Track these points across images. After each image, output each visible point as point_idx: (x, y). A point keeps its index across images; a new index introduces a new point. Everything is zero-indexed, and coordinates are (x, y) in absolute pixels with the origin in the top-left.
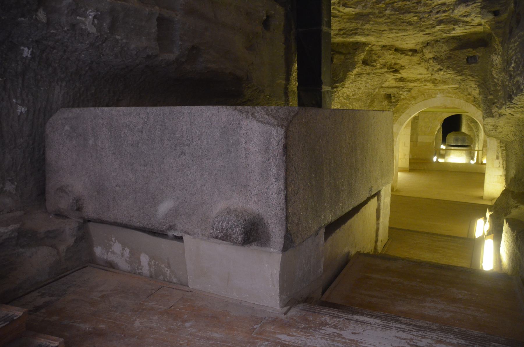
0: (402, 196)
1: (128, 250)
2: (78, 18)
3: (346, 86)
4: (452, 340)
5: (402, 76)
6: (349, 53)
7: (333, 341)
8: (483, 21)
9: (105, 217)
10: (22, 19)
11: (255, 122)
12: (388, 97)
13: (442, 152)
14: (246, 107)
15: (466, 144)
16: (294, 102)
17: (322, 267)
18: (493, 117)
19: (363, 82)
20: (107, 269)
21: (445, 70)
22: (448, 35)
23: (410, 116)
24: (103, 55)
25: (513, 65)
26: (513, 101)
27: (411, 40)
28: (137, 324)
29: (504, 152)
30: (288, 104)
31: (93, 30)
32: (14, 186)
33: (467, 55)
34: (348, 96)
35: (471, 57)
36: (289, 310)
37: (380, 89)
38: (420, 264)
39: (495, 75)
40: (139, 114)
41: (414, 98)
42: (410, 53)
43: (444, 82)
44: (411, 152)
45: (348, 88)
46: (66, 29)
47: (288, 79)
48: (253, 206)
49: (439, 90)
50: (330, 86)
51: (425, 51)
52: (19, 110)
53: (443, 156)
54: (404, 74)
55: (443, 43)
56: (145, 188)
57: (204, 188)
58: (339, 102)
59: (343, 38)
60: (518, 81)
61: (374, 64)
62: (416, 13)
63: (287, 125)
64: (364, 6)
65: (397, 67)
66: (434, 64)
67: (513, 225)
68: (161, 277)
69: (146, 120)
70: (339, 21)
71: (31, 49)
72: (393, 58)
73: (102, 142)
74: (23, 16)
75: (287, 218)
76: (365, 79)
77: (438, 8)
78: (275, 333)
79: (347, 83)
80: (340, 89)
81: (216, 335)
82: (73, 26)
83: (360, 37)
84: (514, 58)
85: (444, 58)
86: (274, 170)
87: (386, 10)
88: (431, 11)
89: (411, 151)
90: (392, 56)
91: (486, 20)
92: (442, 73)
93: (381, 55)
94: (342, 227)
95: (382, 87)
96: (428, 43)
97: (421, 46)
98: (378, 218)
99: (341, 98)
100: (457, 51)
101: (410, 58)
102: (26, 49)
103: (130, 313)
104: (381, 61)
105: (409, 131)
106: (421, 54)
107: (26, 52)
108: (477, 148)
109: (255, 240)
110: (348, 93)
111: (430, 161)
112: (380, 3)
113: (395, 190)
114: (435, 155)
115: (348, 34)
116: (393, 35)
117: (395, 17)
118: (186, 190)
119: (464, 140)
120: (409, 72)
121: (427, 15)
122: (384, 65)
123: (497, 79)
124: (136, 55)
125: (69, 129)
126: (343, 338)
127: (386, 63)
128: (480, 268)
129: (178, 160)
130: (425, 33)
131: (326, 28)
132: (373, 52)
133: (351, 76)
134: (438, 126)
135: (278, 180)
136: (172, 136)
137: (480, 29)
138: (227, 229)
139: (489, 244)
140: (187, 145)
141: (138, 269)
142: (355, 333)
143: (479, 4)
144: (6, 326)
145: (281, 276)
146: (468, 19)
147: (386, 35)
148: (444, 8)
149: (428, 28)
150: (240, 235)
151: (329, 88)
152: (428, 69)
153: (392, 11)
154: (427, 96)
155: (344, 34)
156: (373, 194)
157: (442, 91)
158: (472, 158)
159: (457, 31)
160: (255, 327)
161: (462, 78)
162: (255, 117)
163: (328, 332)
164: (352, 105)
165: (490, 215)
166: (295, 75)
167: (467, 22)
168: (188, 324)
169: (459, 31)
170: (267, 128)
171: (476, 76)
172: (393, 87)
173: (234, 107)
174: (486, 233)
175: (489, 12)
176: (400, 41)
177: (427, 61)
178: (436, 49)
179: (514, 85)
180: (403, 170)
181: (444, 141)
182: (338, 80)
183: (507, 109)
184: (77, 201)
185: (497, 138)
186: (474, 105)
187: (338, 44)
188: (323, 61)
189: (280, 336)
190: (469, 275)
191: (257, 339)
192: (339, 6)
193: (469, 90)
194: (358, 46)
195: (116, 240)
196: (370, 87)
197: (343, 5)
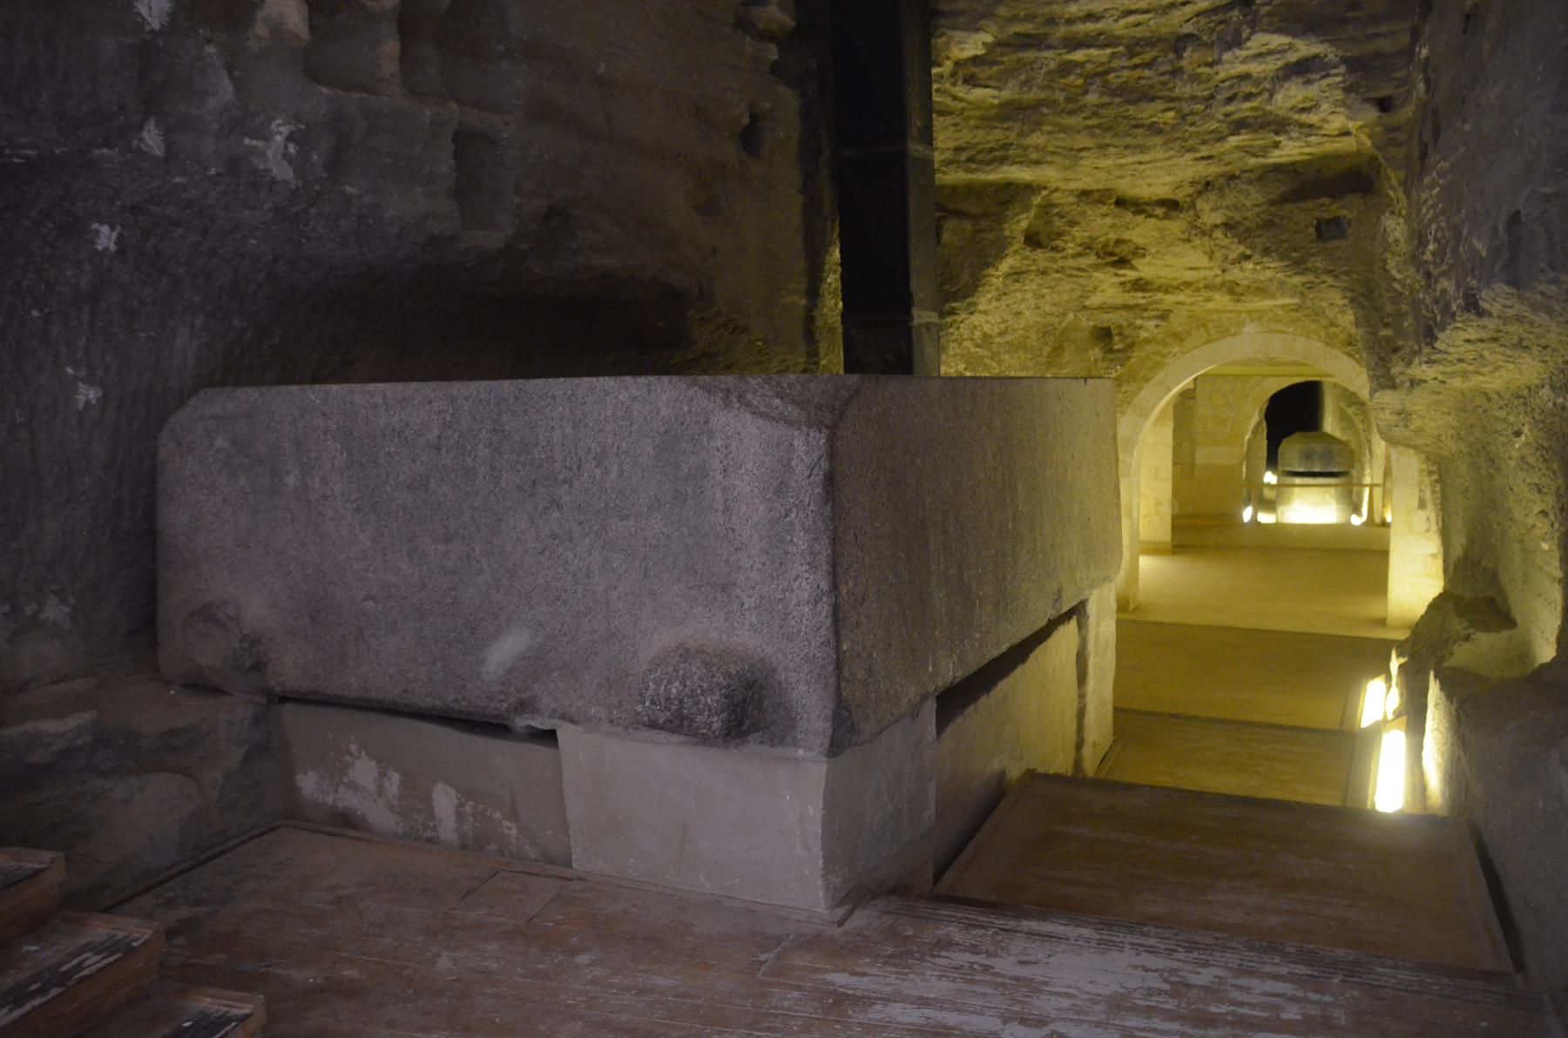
0: (1154, 623)
1: (396, 778)
2: (247, 141)
3: (981, 307)
4: (1276, 969)
5: (1142, 275)
6: (986, 215)
7: (972, 982)
8: (1352, 126)
9: (351, 682)
10: (105, 151)
11: (748, 416)
12: (1104, 335)
13: (1268, 494)
14: (722, 378)
15: (1336, 469)
16: (833, 357)
17: (933, 805)
18: (1394, 387)
19: (1029, 295)
20: (336, 830)
21: (1257, 257)
22: (1261, 160)
23: (1169, 390)
24: (309, 239)
25: (1431, 247)
26: (1437, 345)
27: (1160, 174)
28: (444, 963)
29: (1438, 488)
30: (816, 363)
31: (283, 172)
32: (66, 609)
33: (1317, 214)
34: (986, 336)
35: (1329, 222)
36: (852, 911)
37: (1080, 315)
38: (1200, 797)
39: (1394, 272)
40: (430, 402)
41: (1178, 337)
42: (1160, 211)
43: (1261, 291)
44: (1175, 495)
45: (985, 312)
46: (213, 171)
47: (813, 293)
48: (746, 637)
49: (1249, 312)
50: (935, 310)
51: (1200, 204)
52: (82, 398)
53: (1270, 506)
54: (1145, 269)
55: (1250, 182)
56: (449, 600)
57: (614, 595)
58: (962, 356)
59: (967, 171)
60: (1444, 292)
61: (1058, 242)
62: (1172, 100)
63: (831, 420)
64: (1025, 83)
65: (1124, 250)
66: (1226, 242)
67: (1448, 687)
68: (493, 847)
69: (448, 418)
70: (956, 125)
71: (118, 229)
72: (1113, 226)
73: (324, 480)
74: (107, 143)
75: (839, 666)
76: (1034, 286)
77: (1232, 86)
78: (816, 970)
79: (982, 300)
80: (963, 316)
81: (660, 981)
82: (234, 165)
83: (1015, 168)
84: (1433, 227)
85: (1253, 225)
86: (801, 541)
87: (1086, 92)
88: (1212, 97)
89: (1176, 494)
90: (1108, 221)
91: (1359, 123)
92: (1249, 265)
93: (1077, 219)
94: (983, 700)
95: (1085, 308)
96: (1208, 184)
97: (1190, 190)
98: (1082, 678)
99: (966, 343)
100: (1287, 207)
101: (1161, 224)
102: (105, 229)
103: (420, 938)
104: (1078, 233)
105: (1167, 432)
106: (1191, 212)
107: (106, 238)
108: (1367, 480)
109: (755, 728)
110: (986, 328)
111: (1233, 520)
112: (1069, 73)
113: (1132, 606)
114: (1247, 502)
115: (981, 162)
116: (1109, 162)
117: (1112, 111)
118: (565, 602)
119: (1328, 456)
120: (1159, 262)
121: (1200, 107)
122: (1087, 247)
123: (1399, 281)
124: (398, 236)
125: (227, 445)
126: (997, 975)
127: (1091, 238)
128: (1369, 806)
129: (540, 522)
130: (1198, 155)
131: (920, 148)
132: (1056, 210)
133: (994, 281)
134: (1254, 417)
135: (813, 566)
136: (522, 458)
137: (1348, 145)
138: (681, 702)
139: (1393, 745)
140: (564, 482)
141: (425, 827)
142: (1027, 963)
143: (1339, 79)
144: (43, 1004)
145: (828, 823)
146: (1312, 118)
147: (1088, 161)
148: (1248, 88)
149: (1204, 142)
150: (717, 714)
151: (933, 317)
152: (1211, 255)
153: (1102, 94)
154: (1213, 329)
155: (970, 160)
156: (1065, 609)
157: (1259, 316)
158: (1356, 509)
159: (1286, 151)
160: (763, 957)
161: (1305, 279)
162: (749, 405)
163: (954, 963)
164: (1000, 362)
165: (1401, 667)
166: (833, 279)
167: (1311, 126)
168: (582, 959)
169: (1290, 150)
170: (779, 431)
171: (1345, 273)
172: (1116, 308)
173: (689, 379)
174: (1390, 717)
175: (1366, 100)
176: (1128, 179)
177: (1205, 233)
178: (1230, 199)
179: (1436, 302)
180: (1154, 549)
181: (1272, 461)
182: (956, 290)
183: (1424, 367)
184: (253, 643)
185: (1416, 448)
186: (1349, 354)
187: (954, 189)
188: (913, 240)
189: (830, 977)
190: (1337, 828)
191: (771, 985)
192: (954, 84)
193: (1330, 313)
194: (1012, 194)
195: (360, 750)
196: (1047, 309)
197: (966, 81)
